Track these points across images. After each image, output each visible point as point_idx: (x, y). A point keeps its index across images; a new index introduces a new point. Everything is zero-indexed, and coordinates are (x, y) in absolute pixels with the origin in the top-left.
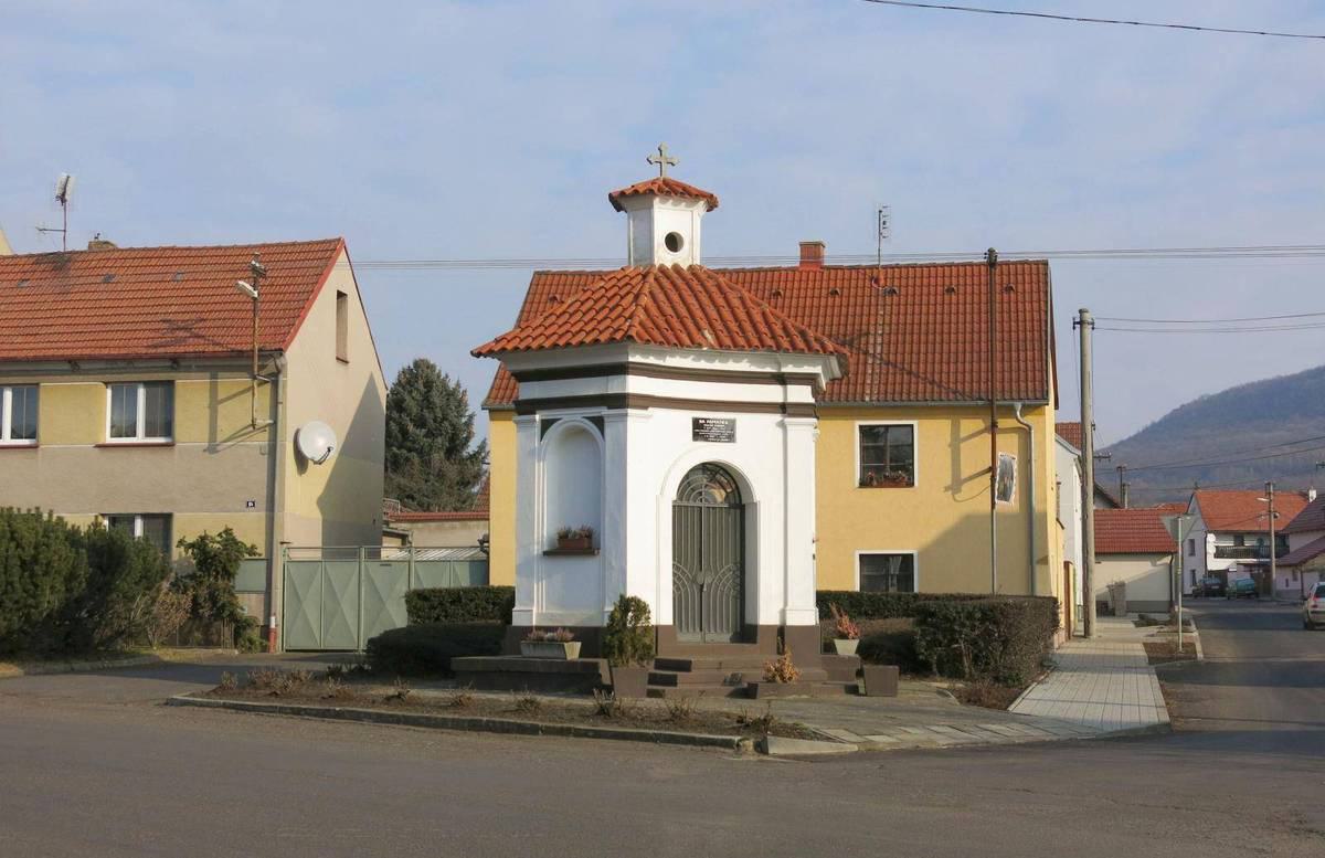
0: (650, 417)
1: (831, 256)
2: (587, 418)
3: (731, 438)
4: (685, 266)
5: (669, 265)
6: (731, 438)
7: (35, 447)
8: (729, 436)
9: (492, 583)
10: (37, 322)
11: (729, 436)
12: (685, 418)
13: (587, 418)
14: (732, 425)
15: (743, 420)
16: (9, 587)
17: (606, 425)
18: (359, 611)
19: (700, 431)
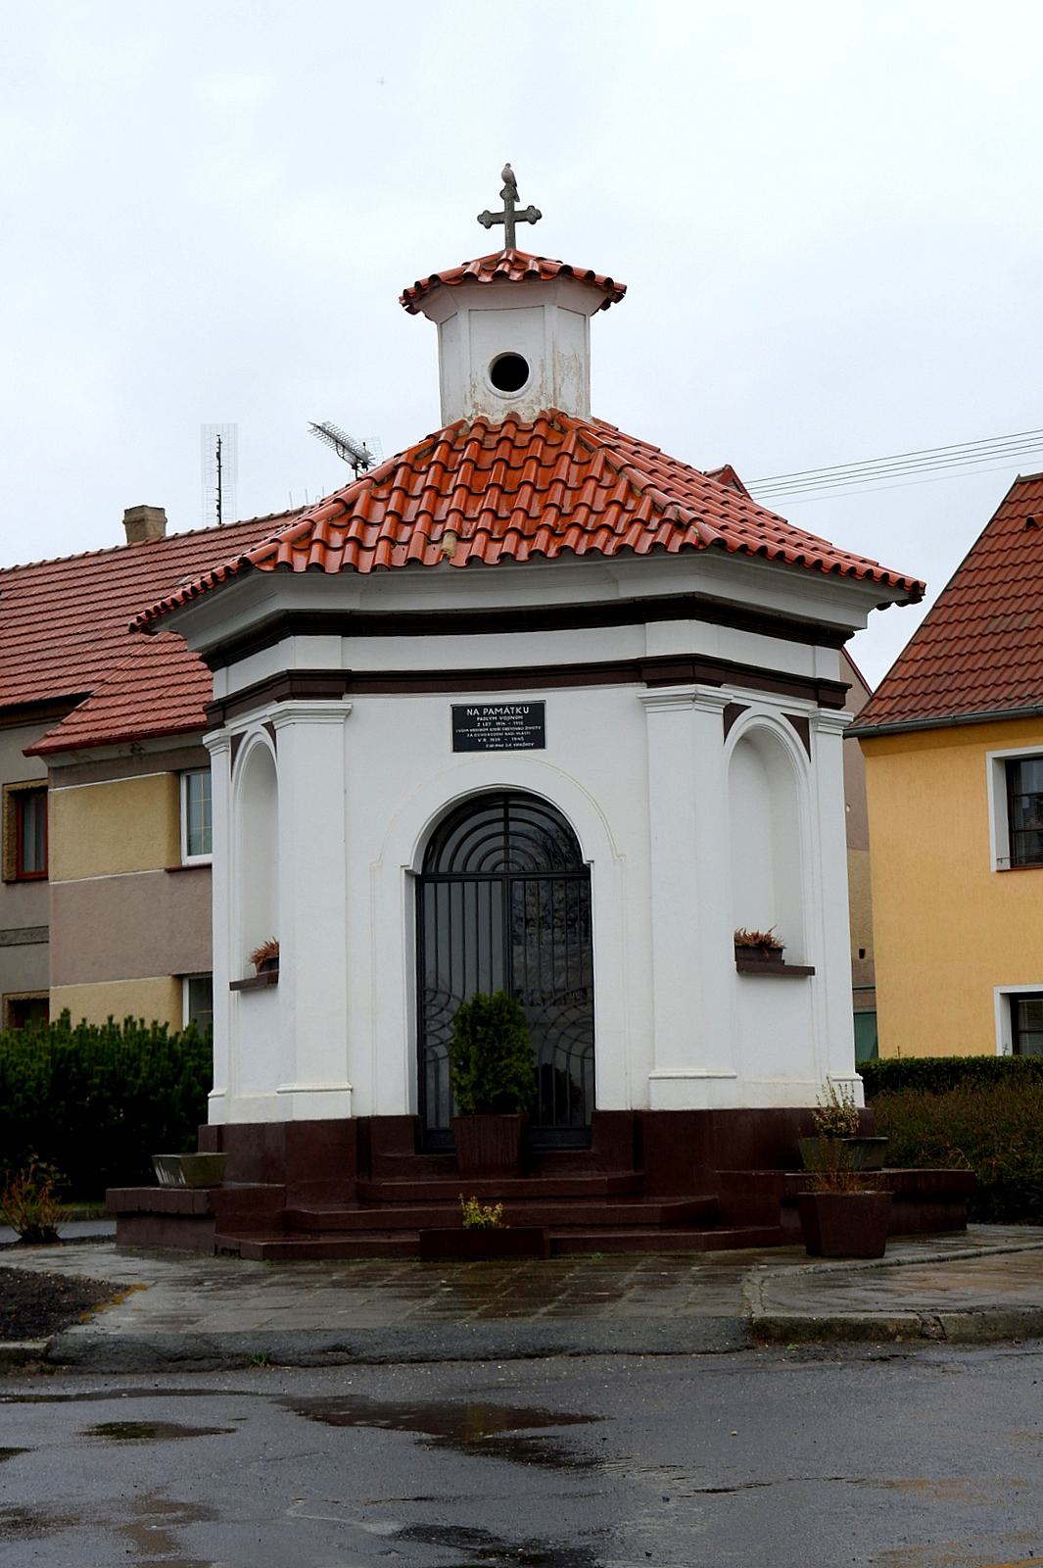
0: (348, 714)
1: (1022, 476)
2: (784, 715)
3: (538, 741)
4: (527, 417)
5: (497, 418)
6: (538, 741)
7: (4, 995)
8: (531, 731)
9: (881, 1056)
10: (22, 583)
11: (531, 731)
12: (438, 708)
13: (784, 715)
14: (537, 712)
15: (558, 703)
16: (65, 1543)
17: (811, 729)
18: (183, 1393)
19: (468, 734)
